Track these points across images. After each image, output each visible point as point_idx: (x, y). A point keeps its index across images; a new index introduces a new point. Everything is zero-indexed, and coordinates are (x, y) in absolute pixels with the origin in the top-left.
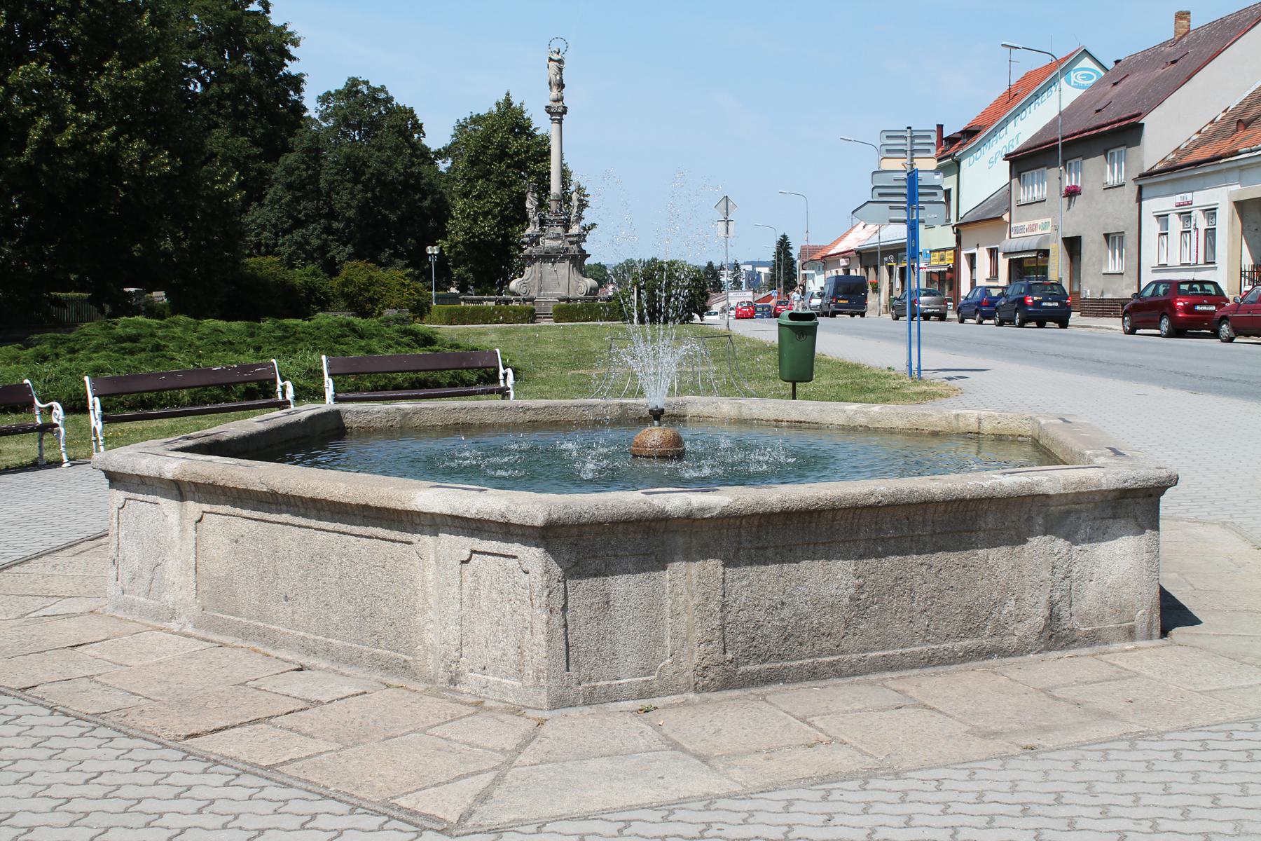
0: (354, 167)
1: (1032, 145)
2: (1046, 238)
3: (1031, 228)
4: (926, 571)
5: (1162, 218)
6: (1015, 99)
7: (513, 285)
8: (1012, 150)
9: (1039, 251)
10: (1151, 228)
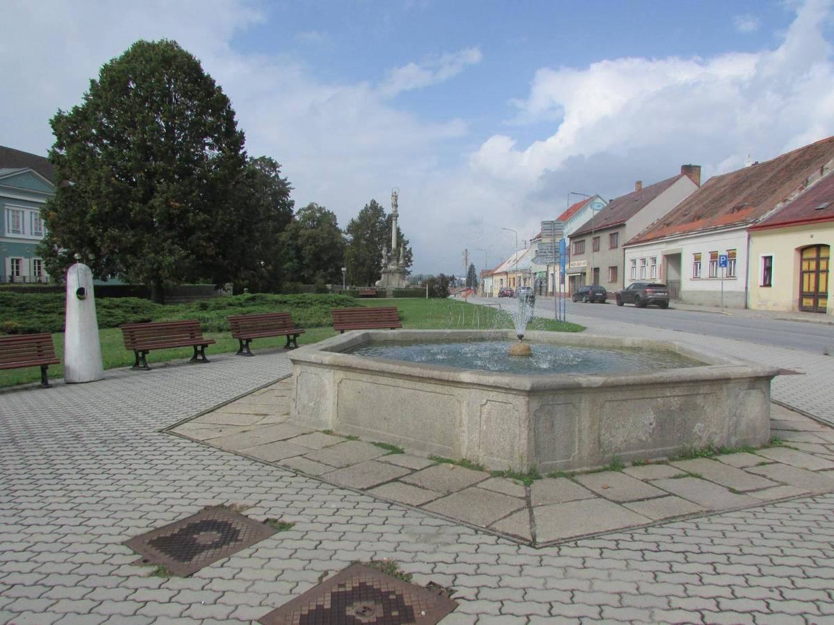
0: (313, 239)
1: (580, 231)
2: (584, 268)
3: (578, 264)
4: (446, 389)
5: (634, 261)
6: (568, 215)
7: (377, 283)
8: (570, 234)
9: (581, 273)
10: (628, 265)
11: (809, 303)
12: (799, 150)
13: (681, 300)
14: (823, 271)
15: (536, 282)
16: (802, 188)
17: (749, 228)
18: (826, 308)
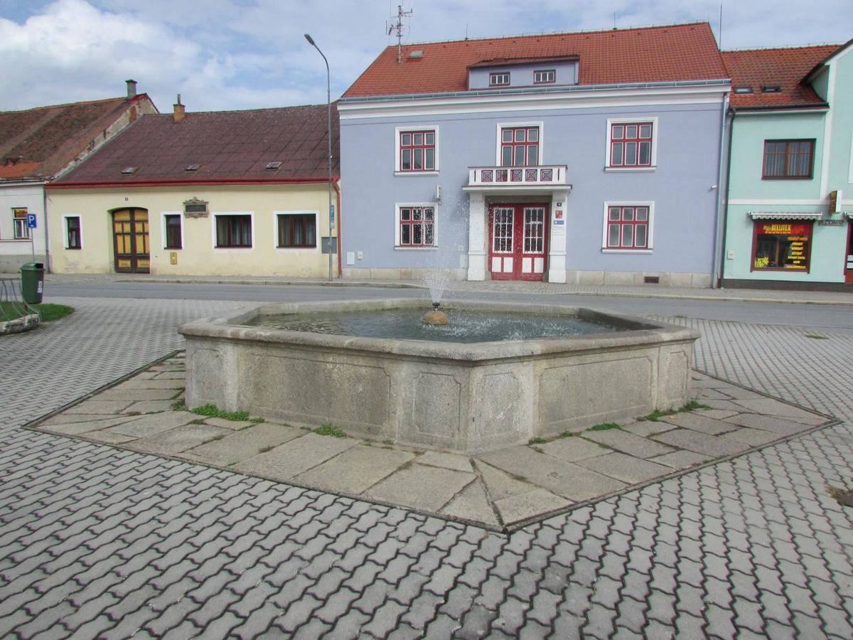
14: (139, 234)
16: (89, 149)
18: (149, 269)
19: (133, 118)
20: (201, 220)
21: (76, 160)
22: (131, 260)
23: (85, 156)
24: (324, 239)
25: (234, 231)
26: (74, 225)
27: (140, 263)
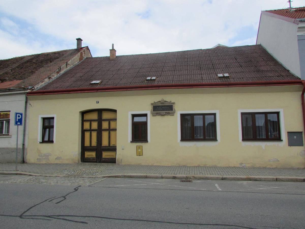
11: (92, 155)
12: (33, 55)
13: (26, 163)
14: (105, 130)
15: (190, 178)
16: (58, 72)
17: (27, 93)
18: (115, 159)
19: (81, 58)
20: (167, 119)
21: (50, 78)
22: (96, 151)
23: (55, 76)
24: (290, 134)
25: (197, 129)
26: (48, 124)
27: (105, 155)
